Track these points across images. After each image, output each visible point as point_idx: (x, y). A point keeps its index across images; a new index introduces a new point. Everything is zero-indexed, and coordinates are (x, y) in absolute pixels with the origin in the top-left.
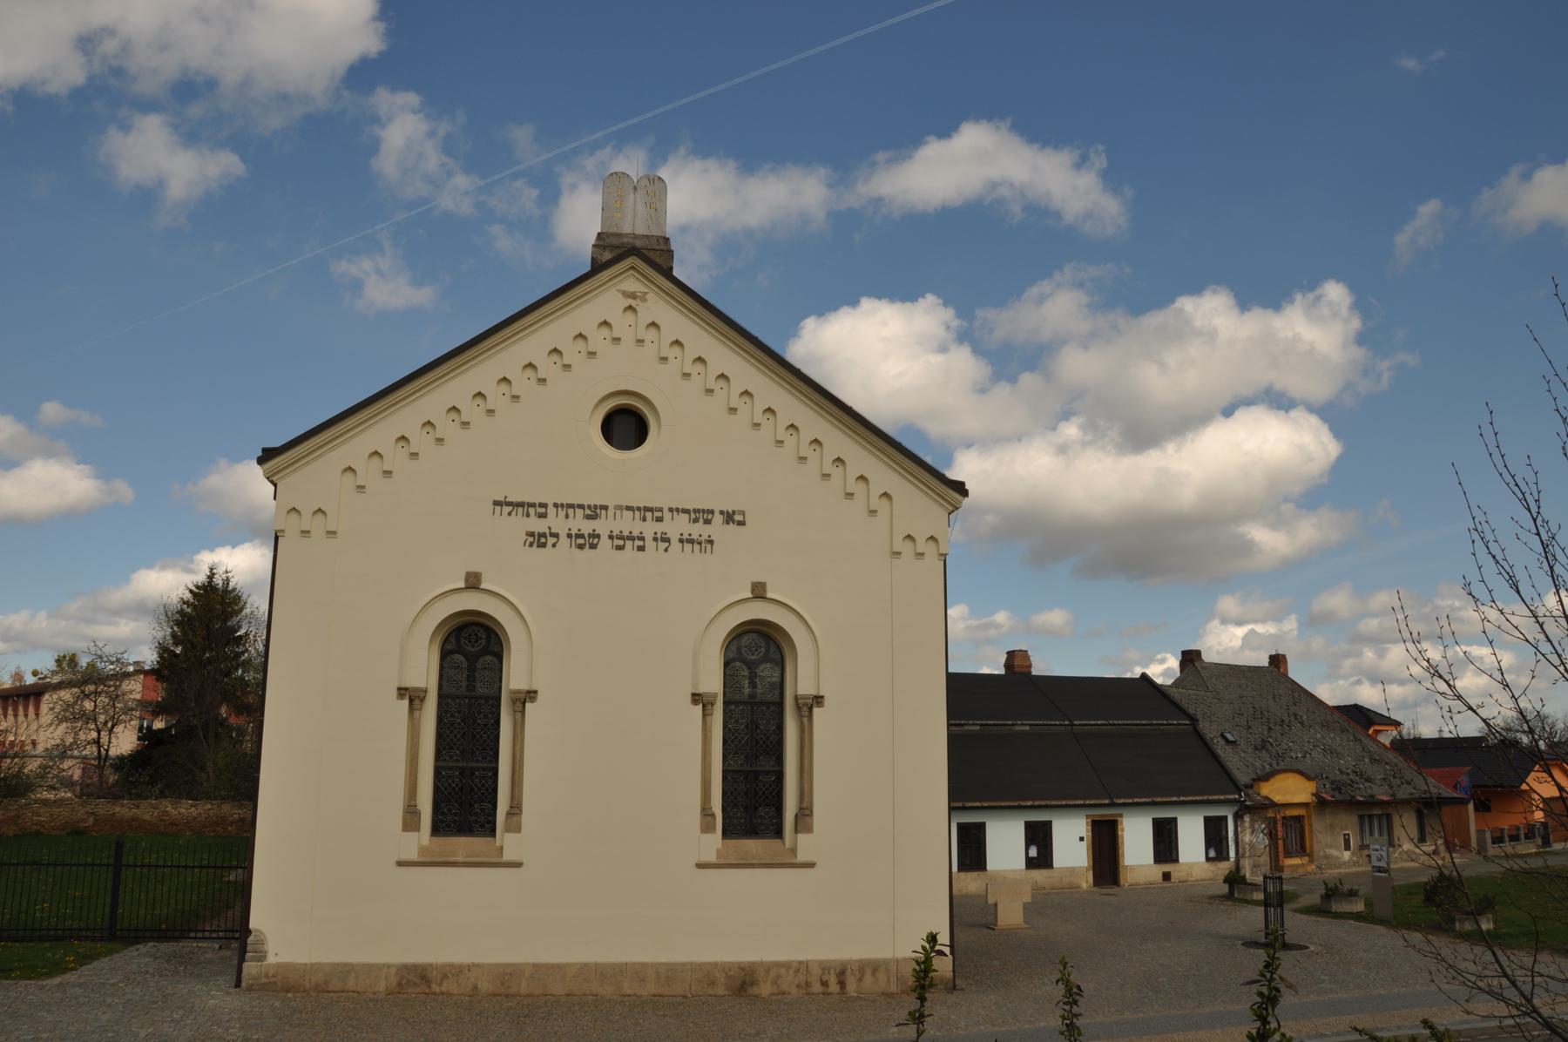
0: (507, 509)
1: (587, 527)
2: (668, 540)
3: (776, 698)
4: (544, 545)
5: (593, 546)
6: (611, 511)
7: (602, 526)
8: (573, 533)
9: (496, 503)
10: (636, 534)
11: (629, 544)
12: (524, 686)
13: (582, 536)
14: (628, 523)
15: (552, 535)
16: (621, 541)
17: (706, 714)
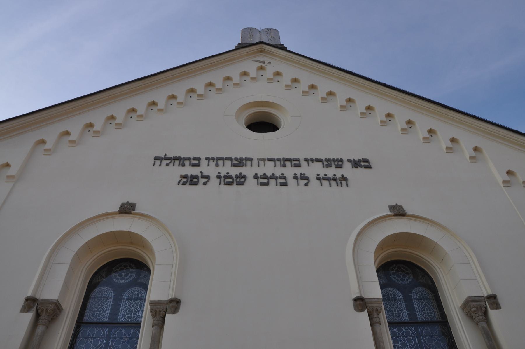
0: (165, 162)
1: (234, 172)
2: (307, 179)
3: (436, 316)
4: (196, 184)
5: (242, 184)
6: (255, 162)
7: (248, 171)
8: (322, 175)
9: (156, 159)
10: (278, 174)
11: (272, 182)
12: (165, 296)
13: (231, 177)
14: (269, 169)
15: (203, 177)
16: (264, 180)
17: (373, 323)
